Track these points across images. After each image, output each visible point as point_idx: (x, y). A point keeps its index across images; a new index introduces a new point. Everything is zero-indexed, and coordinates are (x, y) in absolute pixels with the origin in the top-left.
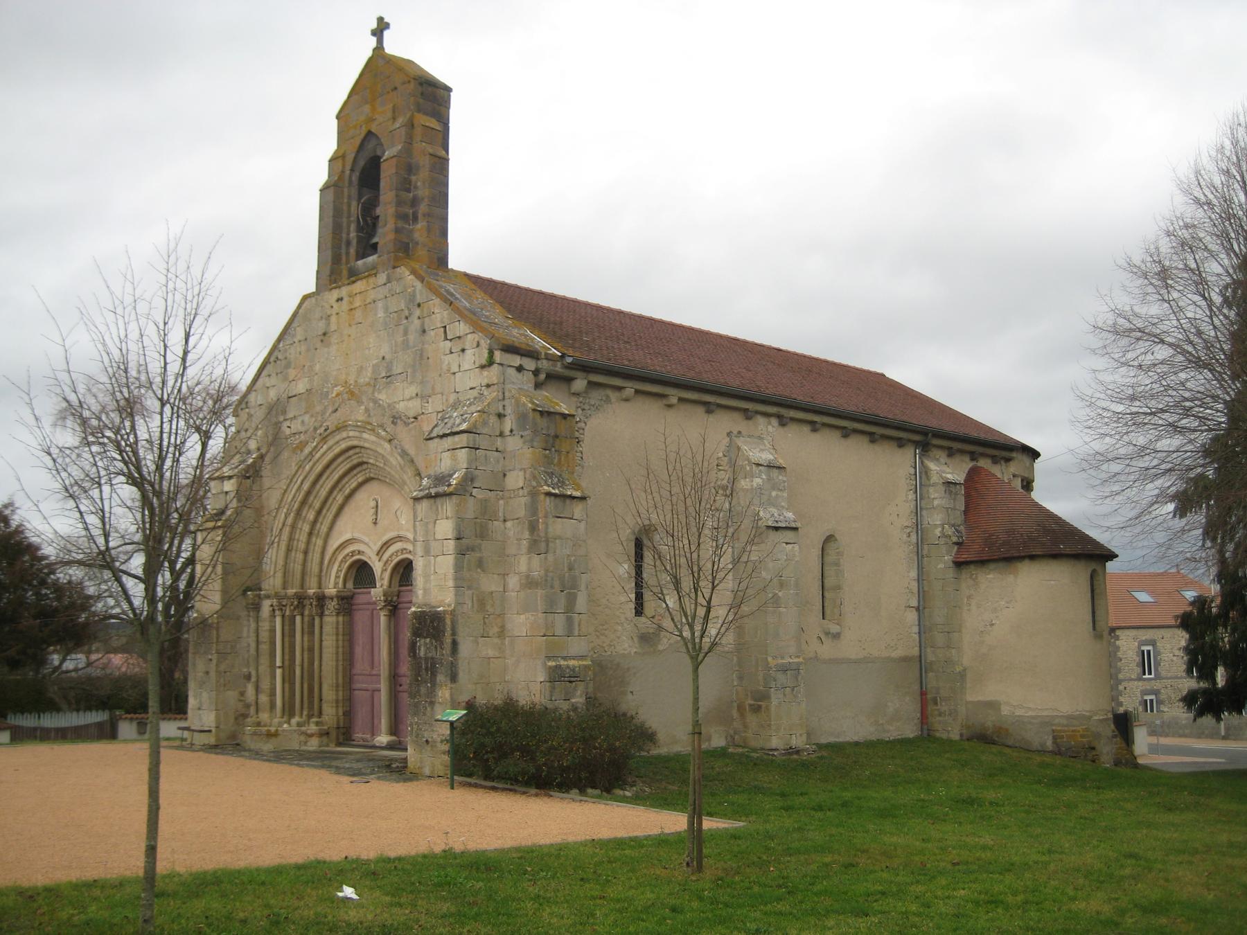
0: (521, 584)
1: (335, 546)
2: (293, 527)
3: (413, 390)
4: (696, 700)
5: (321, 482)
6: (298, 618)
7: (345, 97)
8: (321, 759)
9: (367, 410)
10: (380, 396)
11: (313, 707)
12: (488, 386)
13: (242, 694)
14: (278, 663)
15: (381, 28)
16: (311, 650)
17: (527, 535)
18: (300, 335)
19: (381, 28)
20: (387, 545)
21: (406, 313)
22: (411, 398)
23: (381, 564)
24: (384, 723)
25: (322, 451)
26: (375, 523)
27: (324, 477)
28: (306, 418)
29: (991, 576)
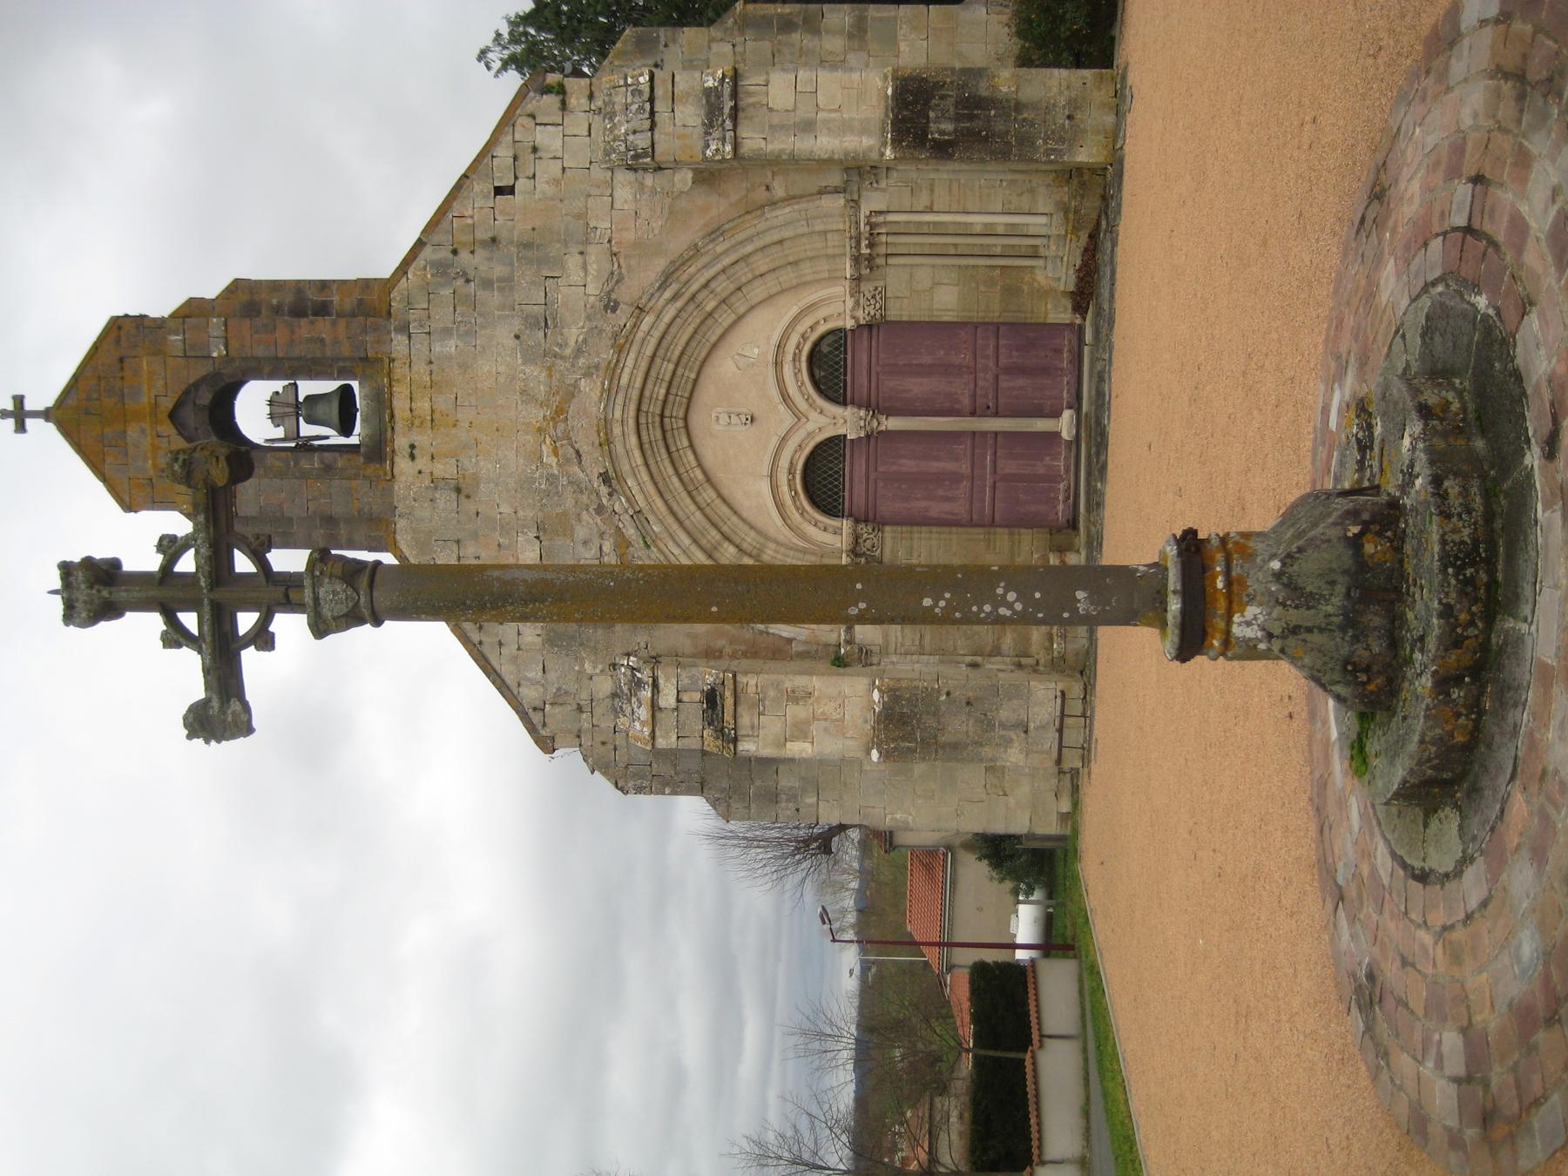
0: (861, 49)
5: (680, 514)
10: (572, 343)
12: (591, 97)
17: (796, 37)
19: (19, 414)
20: (785, 396)
21: (460, 282)
22: (585, 267)
23: (813, 415)
24: (1041, 425)
27: (675, 507)
28: (581, 532)
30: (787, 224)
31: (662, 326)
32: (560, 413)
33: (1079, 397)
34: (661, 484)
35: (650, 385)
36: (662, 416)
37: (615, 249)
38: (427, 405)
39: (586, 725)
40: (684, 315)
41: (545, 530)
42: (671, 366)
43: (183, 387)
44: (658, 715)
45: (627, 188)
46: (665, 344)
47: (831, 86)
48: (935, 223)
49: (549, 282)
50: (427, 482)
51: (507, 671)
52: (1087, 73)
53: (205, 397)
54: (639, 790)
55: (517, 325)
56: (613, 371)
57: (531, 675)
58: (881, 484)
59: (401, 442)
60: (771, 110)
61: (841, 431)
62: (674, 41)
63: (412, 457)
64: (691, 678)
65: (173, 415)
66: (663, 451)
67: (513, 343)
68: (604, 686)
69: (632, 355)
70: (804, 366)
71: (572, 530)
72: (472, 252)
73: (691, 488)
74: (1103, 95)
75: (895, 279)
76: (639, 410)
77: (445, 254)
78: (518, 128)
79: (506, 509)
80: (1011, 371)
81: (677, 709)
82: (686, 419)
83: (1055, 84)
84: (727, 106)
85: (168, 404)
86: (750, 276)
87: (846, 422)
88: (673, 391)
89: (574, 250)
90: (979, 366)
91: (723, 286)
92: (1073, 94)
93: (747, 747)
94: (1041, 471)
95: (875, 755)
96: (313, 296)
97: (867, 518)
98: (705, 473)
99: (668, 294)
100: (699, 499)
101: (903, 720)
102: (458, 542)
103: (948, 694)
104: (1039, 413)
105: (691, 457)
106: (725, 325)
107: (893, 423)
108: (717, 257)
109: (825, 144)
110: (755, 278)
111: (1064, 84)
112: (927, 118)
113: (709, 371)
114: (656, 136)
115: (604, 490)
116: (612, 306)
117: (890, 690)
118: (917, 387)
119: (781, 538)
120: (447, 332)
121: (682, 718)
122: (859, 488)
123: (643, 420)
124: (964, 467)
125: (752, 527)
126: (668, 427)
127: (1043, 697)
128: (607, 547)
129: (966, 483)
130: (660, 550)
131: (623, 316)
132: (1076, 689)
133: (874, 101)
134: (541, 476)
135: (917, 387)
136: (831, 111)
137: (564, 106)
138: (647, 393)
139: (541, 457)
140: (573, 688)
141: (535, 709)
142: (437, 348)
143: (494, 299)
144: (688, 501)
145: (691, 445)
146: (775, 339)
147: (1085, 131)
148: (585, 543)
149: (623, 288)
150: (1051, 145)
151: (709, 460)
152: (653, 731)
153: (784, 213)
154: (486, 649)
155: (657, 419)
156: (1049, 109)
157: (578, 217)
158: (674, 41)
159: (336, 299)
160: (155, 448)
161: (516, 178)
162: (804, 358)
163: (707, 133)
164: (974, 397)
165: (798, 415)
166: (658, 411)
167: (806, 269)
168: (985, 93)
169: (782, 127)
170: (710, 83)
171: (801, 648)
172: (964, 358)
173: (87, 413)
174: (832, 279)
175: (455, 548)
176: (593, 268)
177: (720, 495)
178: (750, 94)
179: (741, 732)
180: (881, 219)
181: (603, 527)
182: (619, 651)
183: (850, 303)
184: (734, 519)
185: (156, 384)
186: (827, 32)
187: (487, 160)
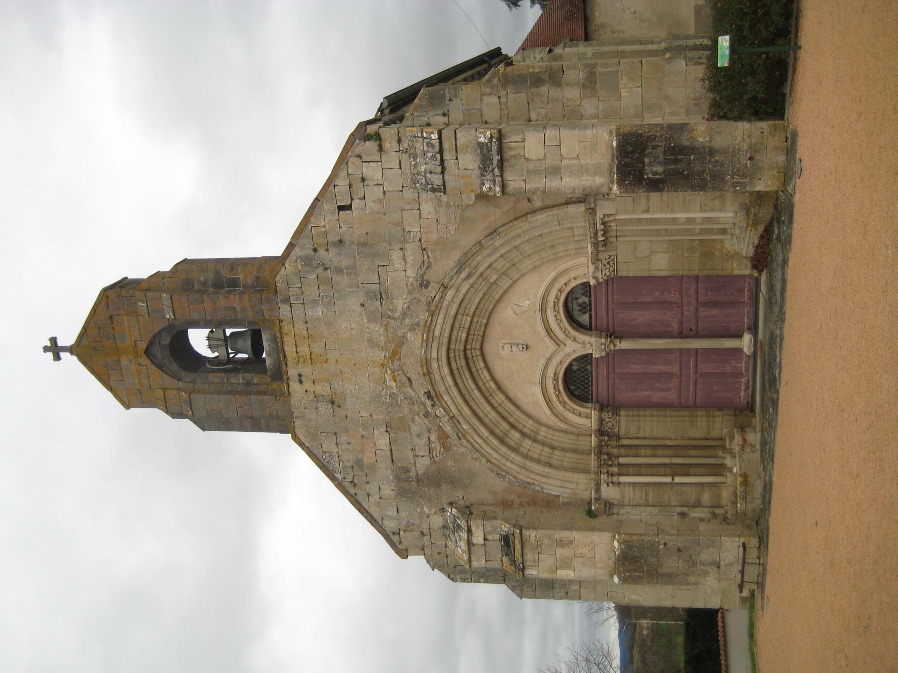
1: (553, 418)
2: (526, 457)
3: (396, 255)
6: (622, 460)
7: (109, 395)
8: (770, 425)
9: (412, 329)
10: (400, 308)
11: (719, 444)
12: (399, 141)
13: (701, 520)
14: (668, 479)
15: (54, 349)
16: (654, 447)
17: (544, 89)
18: (329, 445)
20: (549, 331)
21: (321, 270)
22: (404, 259)
23: (569, 342)
24: (729, 344)
28: (415, 429)
29: (597, 14)
31: (461, 297)
32: (395, 354)
34: (467, 396)
35: (455, 333)
38: (307, 349)
39: (427, 543)
41: (391, 428)
42: (469, 319)
43: (151, 335)
44: (472, 548)
45: (430, 203)
46: (464, 305)
47: (571, 140)
49: (381, 269)
50: (312, 397)
51: (374, 511)
52: (765, 125)
53: (166, 340)
54: (464, 580)
55: (362, 298)
56: (429, 328)
57: (389, 513)
58: (617, 381)
59: (292, 372)
60: (527, 159)
62: (456, 96)
63: (301, 382)
64: (492, 527)
65: (147, 352)
66: (467, 373)
67: (359, 309)
68: (437, 521)
69: (441, 316)
72: (327, 250)
73: (487, 394)
74: (776, 141)
76: (448, 349)
77: (309, 252)
78: (350, 165)
79: (365, 414)
80: (706, 304)
81: (484, 544)
82: (481, 349)
83: (740, 133)
84: (496, 157)
85: (143, 345)
87: (591, 345)
88: (472, 333)
89: (397, 247)
90: (685, 302)
92: (754, 141)
93: (531, 572)
95: (616, 579)
96: (226, 274)
98: (497, 384)
99: (463, 275)
100: (493, 402)
101: (634, 560)
102: (336, 434)
103: (665, 544)
107: (624, 345)
108: (496, 249)
109: (569, 183)
111: (747, 133)
112: (644, 161)
113: (495, 316)
114: (446, 178)
115: (428, 403)
117: (625, 541)
119: (550, 423)
120: (315, 303)
121: (488, 550)
122: (603, 384)
123: (452, 355)
125: (530, 417)
126: (470, 356)
127: (730, 548)
128: (433, 437)
129: (675, 380)
130: (468, 441)
131: (432, 290)
132: (753, 542)
133: (604, 148)
134: (386, 394)
135: (641, 317)
136: (571, 159)
137: (381, 149)
138: (454, 338)
139: (385, 382)
140: (417, 522)
141: (394, 533)
142: (310, 313)
143: (343, 281)
144: (486, 405)
145: (487, 367)
146: (540, 294)
147: (762, 168)
148: (418, 435)
150: (737, 179)
151: (499, 373)
152: (470, 558)
153: (542, 217)
154: (359, 498)
155: (462, 353)
156: (735, 152)
157: (397, 224)
158: (456, 96)
159: (241, 276)
160: (139, 373)
161: (352, 199)
163: (482, 175)
164: (681, 323)
165: (558, 343)
166: (462, 348)
168: (686, 143)
169: (537, 172)
170: (482, 140)
171: (565, 500)
172: (674, 297)
173: (95, 349)
174: (579, 252)
175: (334, 438)
176: (410, 259)
177: (508, 398)
178: (511, 149)
179: (527, 564)
181: (430, 426)
182: (445, 501)
183: (592, 268)
184: (518, 413)
185: (135, 333)
186: (567, 85)
187: (331, 188)
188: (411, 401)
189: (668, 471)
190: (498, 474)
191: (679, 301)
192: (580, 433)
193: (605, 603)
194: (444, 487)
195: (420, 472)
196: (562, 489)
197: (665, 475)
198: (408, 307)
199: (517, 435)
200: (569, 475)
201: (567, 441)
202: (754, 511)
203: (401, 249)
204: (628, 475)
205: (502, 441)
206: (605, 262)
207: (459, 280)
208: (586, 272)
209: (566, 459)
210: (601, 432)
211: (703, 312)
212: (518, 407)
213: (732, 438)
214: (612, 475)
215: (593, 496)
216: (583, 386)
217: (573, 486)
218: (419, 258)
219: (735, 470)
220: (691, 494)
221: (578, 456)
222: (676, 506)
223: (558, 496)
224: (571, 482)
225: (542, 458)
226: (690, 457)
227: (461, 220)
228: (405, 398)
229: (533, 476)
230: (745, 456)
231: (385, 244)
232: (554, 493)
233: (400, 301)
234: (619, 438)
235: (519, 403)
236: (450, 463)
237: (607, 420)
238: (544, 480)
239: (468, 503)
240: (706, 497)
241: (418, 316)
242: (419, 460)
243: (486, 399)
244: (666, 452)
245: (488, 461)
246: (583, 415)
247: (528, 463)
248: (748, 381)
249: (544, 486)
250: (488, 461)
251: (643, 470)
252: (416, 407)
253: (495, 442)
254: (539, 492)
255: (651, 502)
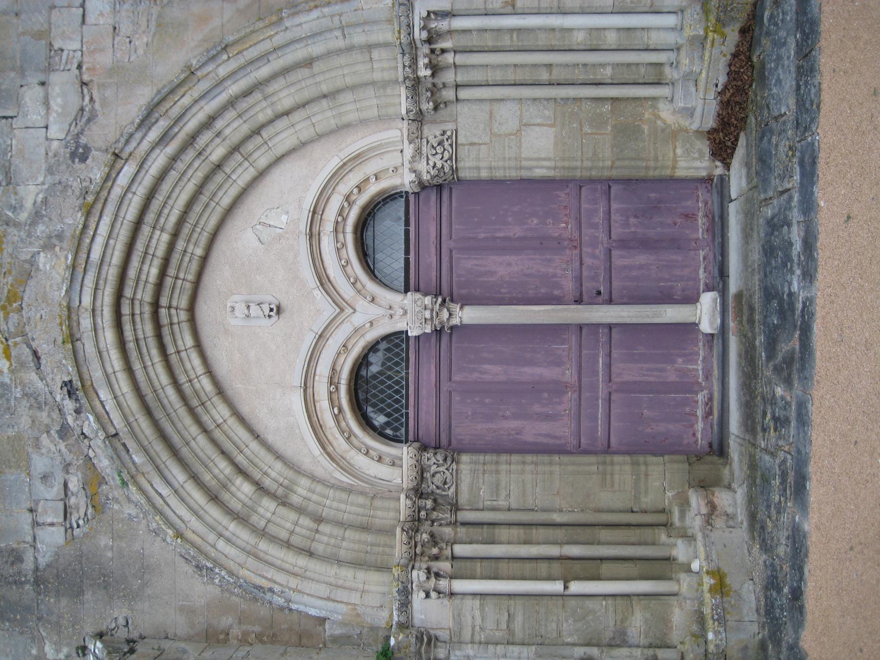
1: (325, 461)
2: (262, 533)
4: (611, 292)
5: (176, 439)
6: (460, 550)
9: (48, 247)
10: (28, 204)
11: (661, 521)
14: (557, 587)
20: (323, 280)
23: (361, 304)
24: (672, 314)
25: (110, 405)
26: (115, 28)
27: (169, 429)
28: (40, 464)
30: (314, 35)
31: (147, 180)
33: (723, 274)
36: (156, 306)
37: (86, 78)
40: (180, 166)
42: (166, 237)
46: (155, 205)
48: (519, 30)
56: (80, 242)
58: (456, 398)
61: (400, 326)
66: (155, 352)
69: (106, 220)
70: (350, 238)
71: (29, 460)
73: (195, 402)
75: (468, 120)
80: (624, 244)
82: (191, 309)
86: (269, 113)
87: (406, 313)
90: (585, 238)
91: (233, 127)
94: (672, 377)
97: (439, 444)
100: (205, 418)
104: (666, 298)
105: (196, 361)
106: (241, 183)
107: (469, 315)
110: (279, 116)
113: (221, 245)
115: (69, 405)
116: (80, 154)
118: (504, 267)
119: (319, 472)
123: (126, 310)
124: (569, 375)
125: (279, 457)
126: (164, 321)
128: (74, 484)
135: (504, 267)
138: (132, 273)
144: (188, 421)
145: (198, 345)
148: (45, 478)
149: (94, 128)
151: (223, 365)
155: (147, 309)
157: (39, 35)
162: (349, 228)
164: (579, 279)
165: (340, 305)
167: (350, 108)
171: (338, 632)
172: (565, 228)
174: (383, 119)
176: (56, 104)
180: (443, 25)
181: (69, 457)
182: (90, 629)
183: (409, 151)
184: (254, 445)
188: (36, 402)
189: (556, 567)
190: (199, 567)
191: (576, 235)
192: (376, 493)
193: (4, 261)
194: (88, 596)
195: (43, 561)
196: (331, 605)
197: (550, 578)
198: (45, 201)
199: (246, 488)
200: (347, 573)
201: (352, 508)
202: (746, 648)
203: (43, 84)
204: (472, 577)
205: (214, 498)
206: (434, 142)
207: (145, 145)
208: (398, 162)
209: (345, 544)
210: (418, 492)
211: (620, 259)
212: (257, 437)
213: (685, 504)
214: (437, 575)
215: (396, 618)
216: (390, 406)
217: (355, 598)
218: (74, 101)
219: (695, 566)
220: (606, 619)
221: (370, 538)
222: (574, 645)
223: (322, 621)
224: (350, 589)
225: (295, 540)
226: (599, 543)
227: (159, 25)
228: (25, 395)
229: (271, 573)
230: (715, 535)
231: (13, 75)
232: (313, 612)
233: (32, 188)
234: (456, 508)
235: (259, 428)
236: (104, 541)
237: (434, 468)
238: (293, 582)
239: (135, 635)
240: (637, 623)
241: (61, 218)
242: (45, 534)
243: (192, 411)
244: (550, 533)
245: (179, 535)
246: (387, 460)
247: (263, 545)
248: (711, 399)
249: (294, 596)
250: (179, 535)
251: (503, 566)
252: (44, 414)
253: (198, 497)
254: (282, 609)
255: (519, 635)
